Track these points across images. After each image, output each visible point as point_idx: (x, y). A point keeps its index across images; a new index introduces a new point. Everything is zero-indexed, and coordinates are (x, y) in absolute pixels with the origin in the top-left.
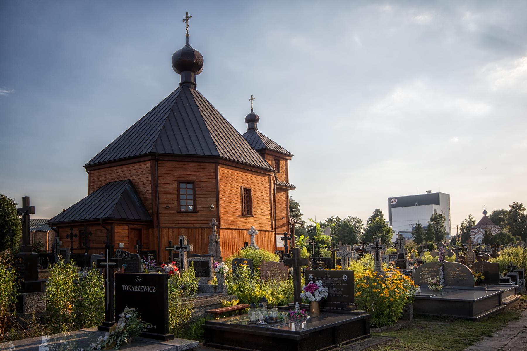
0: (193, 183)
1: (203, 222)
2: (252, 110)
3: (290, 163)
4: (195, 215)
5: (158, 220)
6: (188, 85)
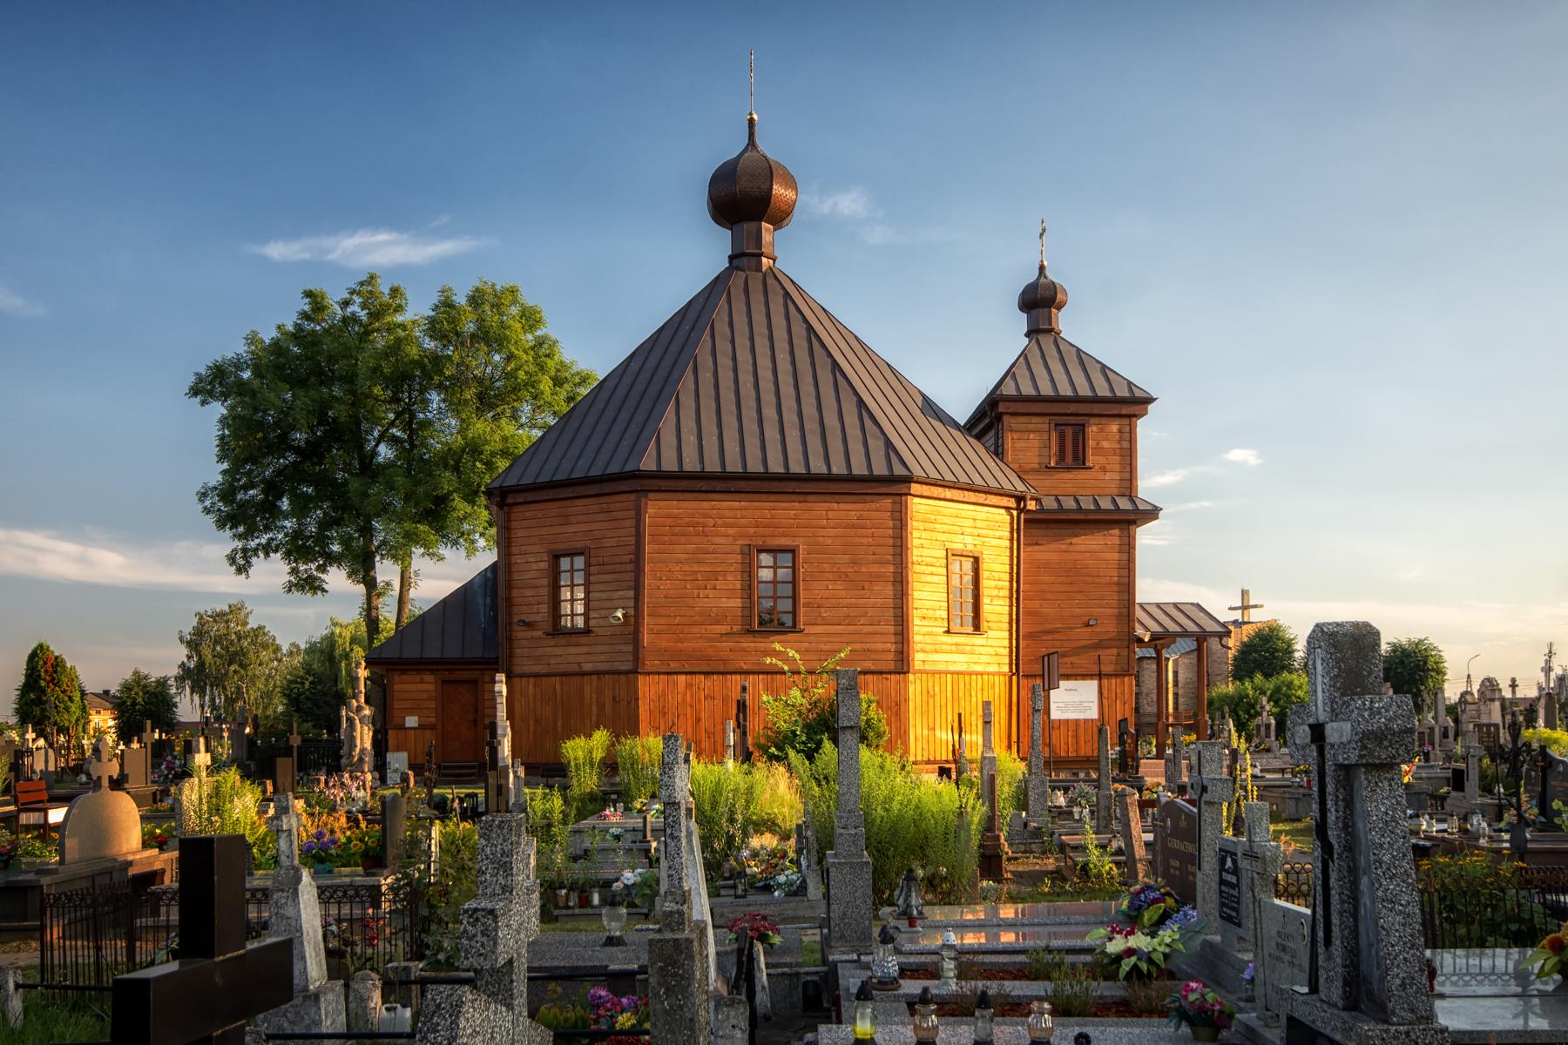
0: (556, 557)
1: (603, 657)
2: (1042, 268)
3: (1147, 430)
4: (584, 640)
5: (511, 656)
6: (745, 257)
